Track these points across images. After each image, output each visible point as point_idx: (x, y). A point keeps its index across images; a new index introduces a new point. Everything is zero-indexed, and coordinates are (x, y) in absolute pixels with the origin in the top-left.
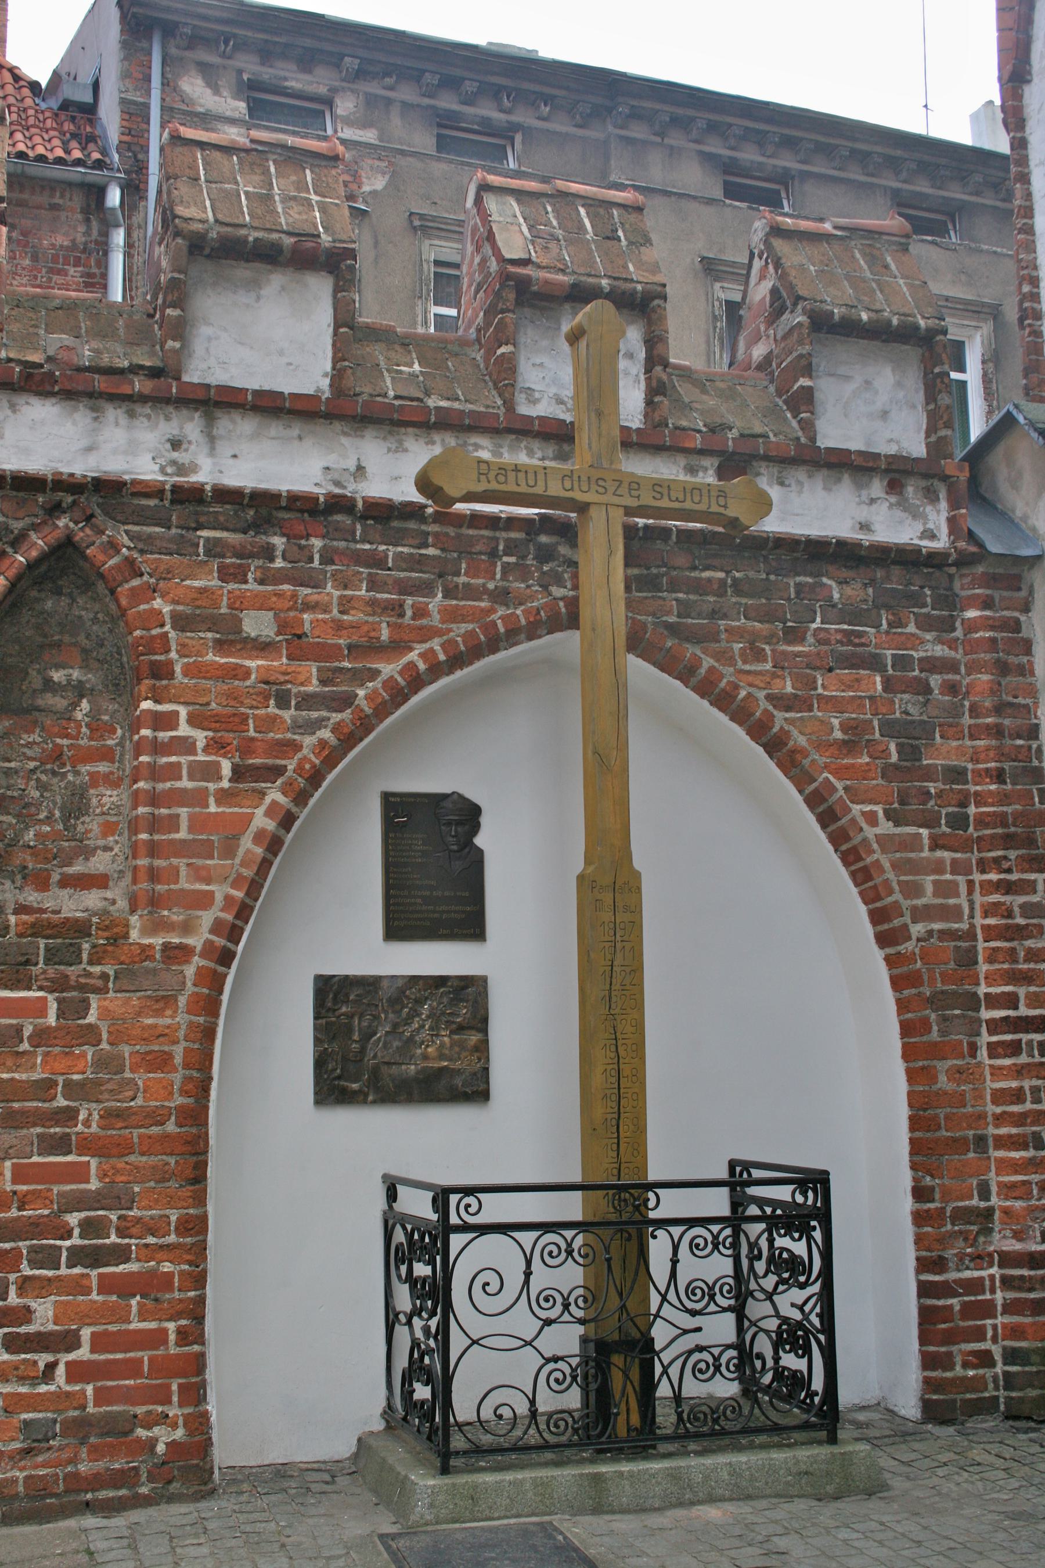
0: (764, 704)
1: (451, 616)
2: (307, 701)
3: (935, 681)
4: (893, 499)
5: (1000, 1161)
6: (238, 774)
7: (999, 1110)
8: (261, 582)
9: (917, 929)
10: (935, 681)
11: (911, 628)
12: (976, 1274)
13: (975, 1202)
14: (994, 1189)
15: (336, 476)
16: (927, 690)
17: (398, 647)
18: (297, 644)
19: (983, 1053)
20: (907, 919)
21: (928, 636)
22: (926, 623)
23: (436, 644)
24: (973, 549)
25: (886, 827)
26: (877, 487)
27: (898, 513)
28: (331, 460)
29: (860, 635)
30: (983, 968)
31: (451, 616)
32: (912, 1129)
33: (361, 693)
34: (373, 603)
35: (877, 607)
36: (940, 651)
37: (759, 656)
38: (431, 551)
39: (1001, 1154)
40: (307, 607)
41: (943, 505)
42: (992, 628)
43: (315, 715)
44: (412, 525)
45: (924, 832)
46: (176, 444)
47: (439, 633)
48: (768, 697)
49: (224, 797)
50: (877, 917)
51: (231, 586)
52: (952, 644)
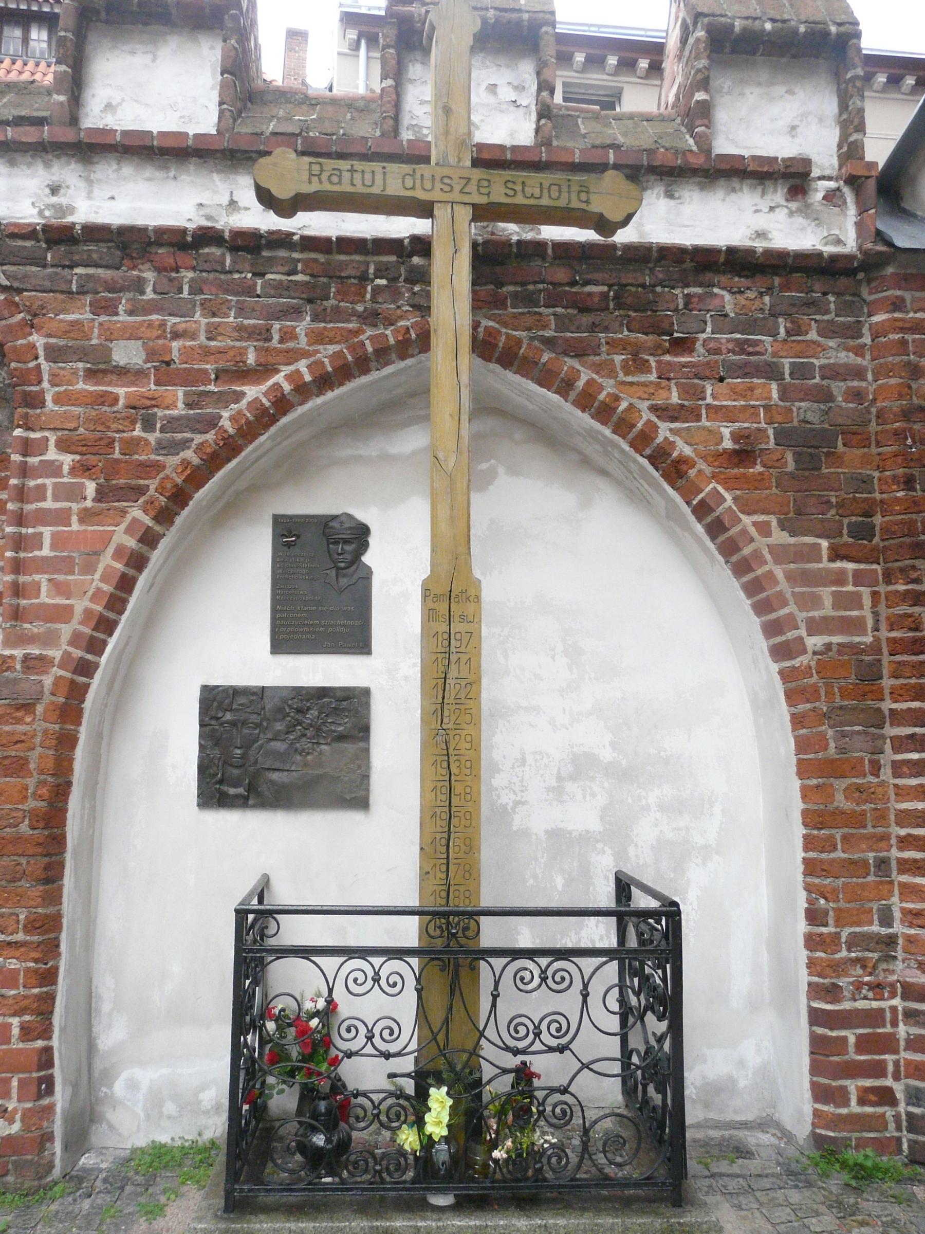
0: (647, 415)
1: (318, 338)
2: (172, 424)
3: (838, 388)
4: (794, 205)
5: (903, 885)
6: (101, 496)
7: (903, 832)
8: (131, 313)
9: (814, 642)
10: (838, 388)
11: (813, 335)
12: (875, 1004)
13: (875, 928)
14: (897, 914)
15: (208, 211)
16: (830, 398)
17: (264, 370)
18: (165, 371)
19: (886, 774)
20: (803, 632)
21: (831, 343)
22: (828, 330)
23: (302, 366)
24: (881, 248)
25: (780, 537)
26: (778, 196)
27: (799, 220)
28: (205, 197)
29: (757, 343)
30: (887, 683)
31: (318, 338)
32: (806, 849)
33: (226, 414)
34: (240, 328)
35: (774, 315)
36: (845, 357)
37: (643, 367)
38: (299, 277)
39: (904, 878)
40: (176, 335)
41: (852, 210)
42: (902, 330)
43: (179, 436)
44: (282, 253)
45: (825, 544)
46: (55, 190)
47: (305, 354)
48: (654, 409)
49: (86, 516)
50: (771, 629)
51: (103, 318)
52: (859, 351)
